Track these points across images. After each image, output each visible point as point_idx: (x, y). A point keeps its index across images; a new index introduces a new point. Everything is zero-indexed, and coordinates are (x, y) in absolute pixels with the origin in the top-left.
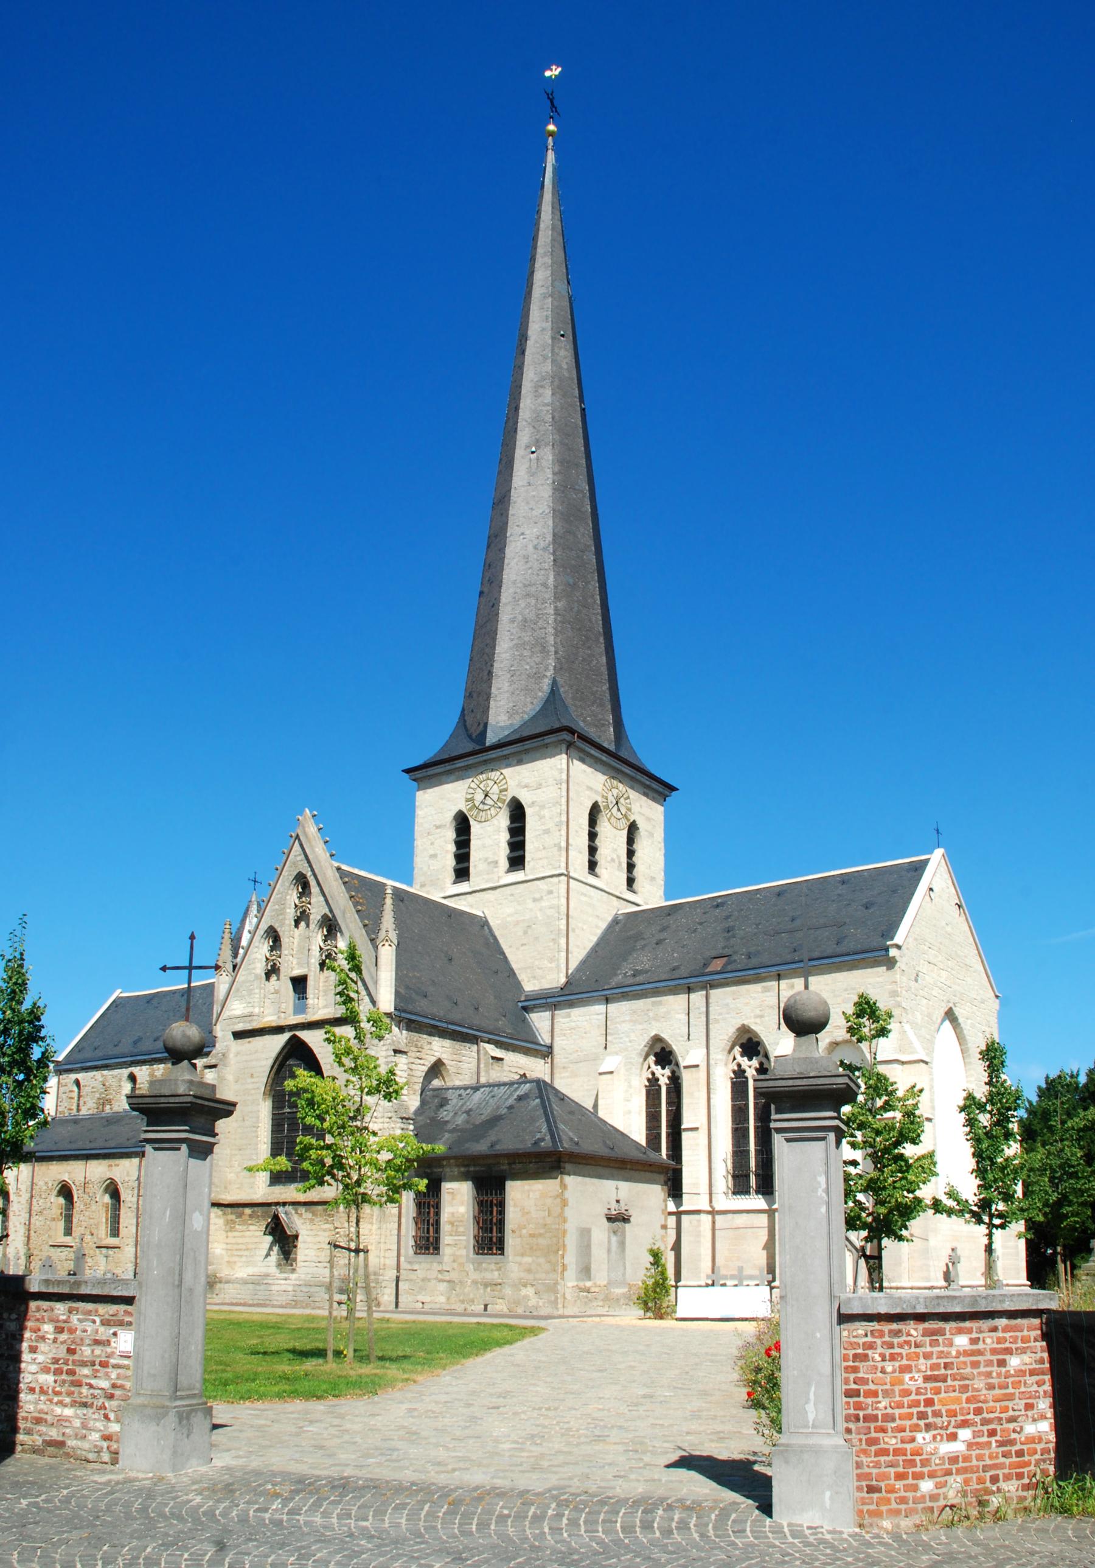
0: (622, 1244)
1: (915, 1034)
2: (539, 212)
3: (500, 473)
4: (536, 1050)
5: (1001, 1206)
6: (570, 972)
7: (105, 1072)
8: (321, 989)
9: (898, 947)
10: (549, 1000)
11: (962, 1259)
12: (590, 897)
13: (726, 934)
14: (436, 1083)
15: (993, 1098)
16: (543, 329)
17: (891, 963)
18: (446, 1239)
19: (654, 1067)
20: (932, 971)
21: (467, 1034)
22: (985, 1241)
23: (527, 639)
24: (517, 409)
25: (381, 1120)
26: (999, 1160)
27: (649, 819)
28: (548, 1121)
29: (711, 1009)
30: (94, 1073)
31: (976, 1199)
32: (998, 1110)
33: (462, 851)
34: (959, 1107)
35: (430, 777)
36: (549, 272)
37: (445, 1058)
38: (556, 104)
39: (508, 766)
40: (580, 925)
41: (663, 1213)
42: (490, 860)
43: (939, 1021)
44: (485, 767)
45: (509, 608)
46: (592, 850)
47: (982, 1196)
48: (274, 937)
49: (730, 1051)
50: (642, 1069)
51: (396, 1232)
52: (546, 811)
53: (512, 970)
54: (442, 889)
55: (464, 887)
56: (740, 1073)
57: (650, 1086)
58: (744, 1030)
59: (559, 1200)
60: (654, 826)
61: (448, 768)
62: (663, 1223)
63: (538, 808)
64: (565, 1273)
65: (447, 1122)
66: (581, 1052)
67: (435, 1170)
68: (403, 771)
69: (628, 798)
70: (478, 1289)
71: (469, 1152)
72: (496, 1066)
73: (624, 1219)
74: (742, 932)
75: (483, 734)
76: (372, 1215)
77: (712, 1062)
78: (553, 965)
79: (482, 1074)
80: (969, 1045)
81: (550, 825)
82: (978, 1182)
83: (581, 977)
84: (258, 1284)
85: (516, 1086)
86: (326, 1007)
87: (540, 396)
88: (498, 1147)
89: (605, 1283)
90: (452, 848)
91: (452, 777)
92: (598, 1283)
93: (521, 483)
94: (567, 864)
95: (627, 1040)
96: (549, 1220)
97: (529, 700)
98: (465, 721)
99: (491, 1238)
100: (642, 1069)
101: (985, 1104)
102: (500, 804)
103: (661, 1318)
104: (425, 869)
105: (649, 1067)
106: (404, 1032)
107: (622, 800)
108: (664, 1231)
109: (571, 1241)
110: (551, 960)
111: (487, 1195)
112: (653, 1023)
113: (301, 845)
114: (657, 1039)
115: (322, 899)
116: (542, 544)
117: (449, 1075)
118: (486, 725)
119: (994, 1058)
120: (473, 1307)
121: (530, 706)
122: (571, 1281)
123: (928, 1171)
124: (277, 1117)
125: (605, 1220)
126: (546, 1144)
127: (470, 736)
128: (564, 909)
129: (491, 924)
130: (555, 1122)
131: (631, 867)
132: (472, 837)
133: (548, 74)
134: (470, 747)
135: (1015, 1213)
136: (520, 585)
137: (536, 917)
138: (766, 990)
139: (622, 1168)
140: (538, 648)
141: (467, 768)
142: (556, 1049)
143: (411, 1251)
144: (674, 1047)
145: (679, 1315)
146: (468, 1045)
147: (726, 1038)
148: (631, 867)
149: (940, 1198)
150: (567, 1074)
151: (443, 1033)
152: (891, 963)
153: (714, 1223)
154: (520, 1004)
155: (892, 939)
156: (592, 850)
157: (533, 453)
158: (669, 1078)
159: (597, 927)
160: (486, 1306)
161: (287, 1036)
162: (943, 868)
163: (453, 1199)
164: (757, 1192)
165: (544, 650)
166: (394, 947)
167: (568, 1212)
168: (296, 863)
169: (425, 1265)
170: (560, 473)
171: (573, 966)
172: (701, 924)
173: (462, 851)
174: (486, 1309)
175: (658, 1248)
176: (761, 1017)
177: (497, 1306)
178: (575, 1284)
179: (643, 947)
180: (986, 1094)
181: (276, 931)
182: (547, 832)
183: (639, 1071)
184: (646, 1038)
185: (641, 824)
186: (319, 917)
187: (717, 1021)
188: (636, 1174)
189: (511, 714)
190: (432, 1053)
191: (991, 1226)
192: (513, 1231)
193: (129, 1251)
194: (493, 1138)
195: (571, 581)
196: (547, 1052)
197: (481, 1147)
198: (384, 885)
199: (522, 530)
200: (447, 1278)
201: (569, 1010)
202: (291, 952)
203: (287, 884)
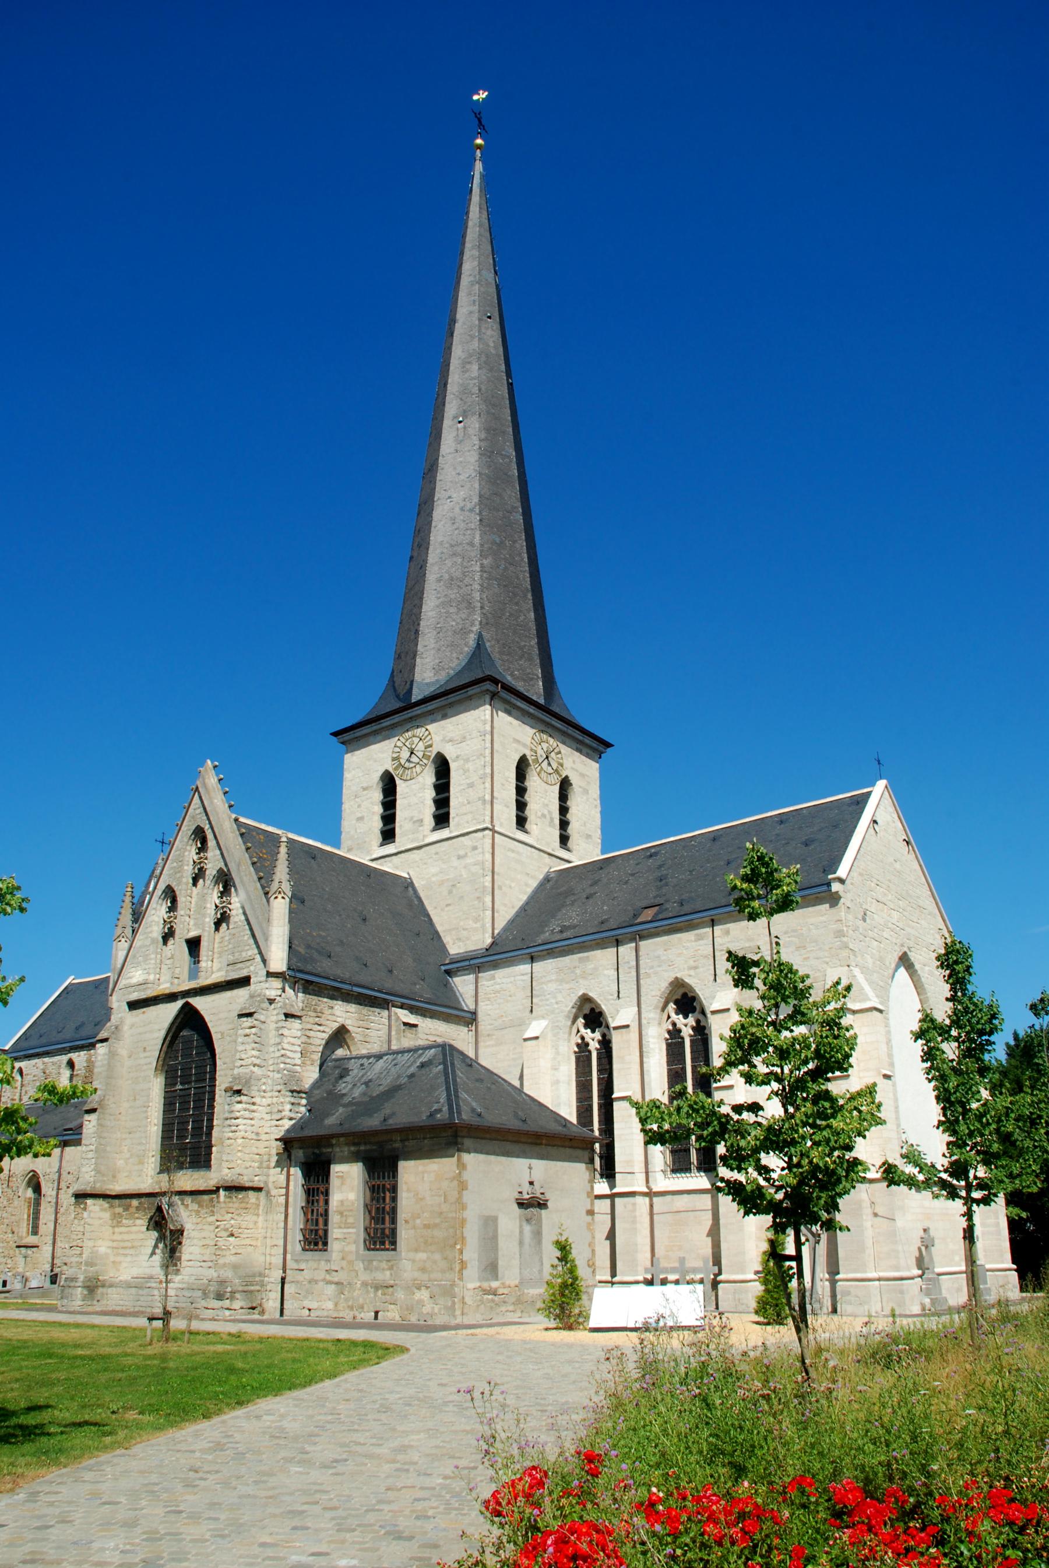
1: (867, 980)
2: (467, 213)
3: (430, 444)
4: (457, 1016)
5: (981, 1172)
6: (496, 932)
7: (46, 1060)
8: (216, 950)
9: (842, 881)
10: (472, 962)
11: (936, 1241)
12: (518, 853)
13: (659, 884)
14: (340, 1052)
15: (958, 1019)
16: (471, 312)
17: (834, 900)
20: (883, 911)
21: (376, 997)
22: (963, 1223)
23: (453, 596)
24: (445, 385)
25: (269, 1094)
26: (974, 1105)
27: (582, 775)
28: (448, 1089)
29: (641, 962)
30: (36, 1061)
31: (946, 1162)
32: (968, 1033)
33: (389, 812)
34: (912, 1032)
35: (357, 739)
36: (476, 263)
37: (350, 1024)
38: (484, 122)
39: (433, 721)
40: (507, 882)
41: (588, 1196)
43: (893, 966)
44: (409, 725)
45: (436, 568)
46: (521, 806)
47: (954, 1158)
48: (171, 895)
49: (663, 1009)
50: (570, 1033)
51: (282, 1225)
52: (470, 764)
53: (437, 932)
54: (369, 852)
55: (390, 849)
56: (675, 1033)
57: (579, 1052)
58: (678, 984)
59: (456, 1182)
60: (589, 783)
61: (375, 728)
62: (589, 1208)
63: (462, 762)
64: (465, 1272)
65: (344, 1095)
67: (324, 1150)
68: (332, 734)
69: (560, 752)
70: (368, 1292)
71: (360, 1128)
72: (409, 1033)
73: (541, 1204)
74: (675, 880)
75: (410, 692)
76: (258, 1205)
77: (644, 1021)
78: (478, 925)
79: (394, 1042)
80: (929, 994)
81: (474, 778)
82: (947, 1138)
83: (507, 937)
84: (141, 1288)
85: (420, 1052)
86: (219, 970)
87: (467, 371)
88: (391, 1121)
89: (517, 1282)
90: (379, 809)
91: (380, 737)
92: (507, 1283)
93: (448, 451)
94: (492, 817)
95: (553, 1001)
96: (445, 1208)
97: (455, 655)
98: (394, 682)
99: (383, 1230)
100: (570, 1033)
101: (950, 1027)
102: (425, 761)
103: (570, 1328)
104: (352, 832)
105: (578, 1031)
106: (300, 995)
107: (553, 755)
108: (590, 1217)
109: (472, 1233)
110: (476, 920)
111: (379, 1178)
112: (581, 981)
113: (200, 798)
114: (585, 999)
115: (218, 852)
116: (469, 506)
117: (355, 1044)
118: (412, 682)
119: (956, 962)
120: (362, 1315)
121: (456, 662)
122: (471, 1282)
123: (868, 1117)
124: (170, 1094)
125: (516, 1206)
126: (442, 1117)
127: (398, 696)
128: (489, 865)
129: (416, 885)
130: (456, 1091)
131: (564, 824)
132: (398, 797)
133: (475, 97)
134: (398, 705)
135: (1002, 1181)
136: (447, 545)
137: (461, 875)
138: (700, 938)
139: (536, 1144)
140: (464, 605)
141: (393, 726)
142: (481, 1016)
143: (298, 1248)
144: (603, 1007)
145: (593, 1323)
146: (378, 1010)
147: (659, 993)
148: (564, 824)
149: (896, 1163)
150: (491, 1043)
151: (347, 997)
152: (834, 900)
153: (651, 1206)
154: (443, 968)
155: (835, 873)
156: (521, 806)
157: (460, 422)
158: (599, 1042)
159: (527, 885)
160: (377, 1313)
161: (179, 1003)
162: (887, 801)
163: (342, 1184)
164: (699, 1169)
165: (470, 605)
166: (288, 900)
167: (467, 1196)
168: (195, 817)
169: (313, 1265)
170: (486, 439)
171: (500, 925)
172: (632, 875)
173: (389, 812)
174: (376, 1317)
175: (566, 1240)
176: (696, 968)
177: (389, 1314)
178: (478, 1284)
179: (573, 903)
180: (950, 1012)
181: (174, 891)
182: (471, 785)
183: (566, 1036)
184: (573, 998)
185: (574, 779)
186: (215, 872)
187: (648, 975)
188: (553, 1151)
189: (436, 670)
190: (334, 1018)
191: (969, 1201)
192: (406, 1222)
193: (47, 1250)
194: (388, 1111)
195: (498, 540)
196: (470, 1019)
197: (373, 1122)
198: (279, 836)
199: (449, 494)
200: (336, 1279)
201: (492, 972)
202: (188, 912)
203: (186, 840)
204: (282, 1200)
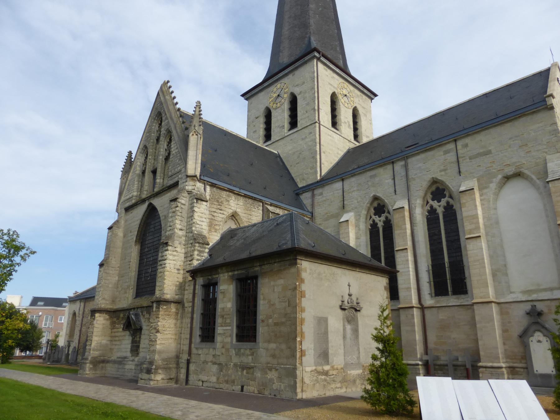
0: (356, 331)
6: (323, 174)
12: (333, 137)
18: (219, 330)
19: (374, 217)
42: (280, 126)
58: (435, 182)
64: (303, 358)
65: (231, 246)
66: (329, 213)
67: (214, 276)
78: (313, 171)
114: (376, 198)
138: (446, 152)
159: (338, 153)
160: (242, 387)
161: (147, 204)
178: (314, 368)
187: (414, 179)
190: (230, 207)
192: (263, 321)
204: (190, 309)
